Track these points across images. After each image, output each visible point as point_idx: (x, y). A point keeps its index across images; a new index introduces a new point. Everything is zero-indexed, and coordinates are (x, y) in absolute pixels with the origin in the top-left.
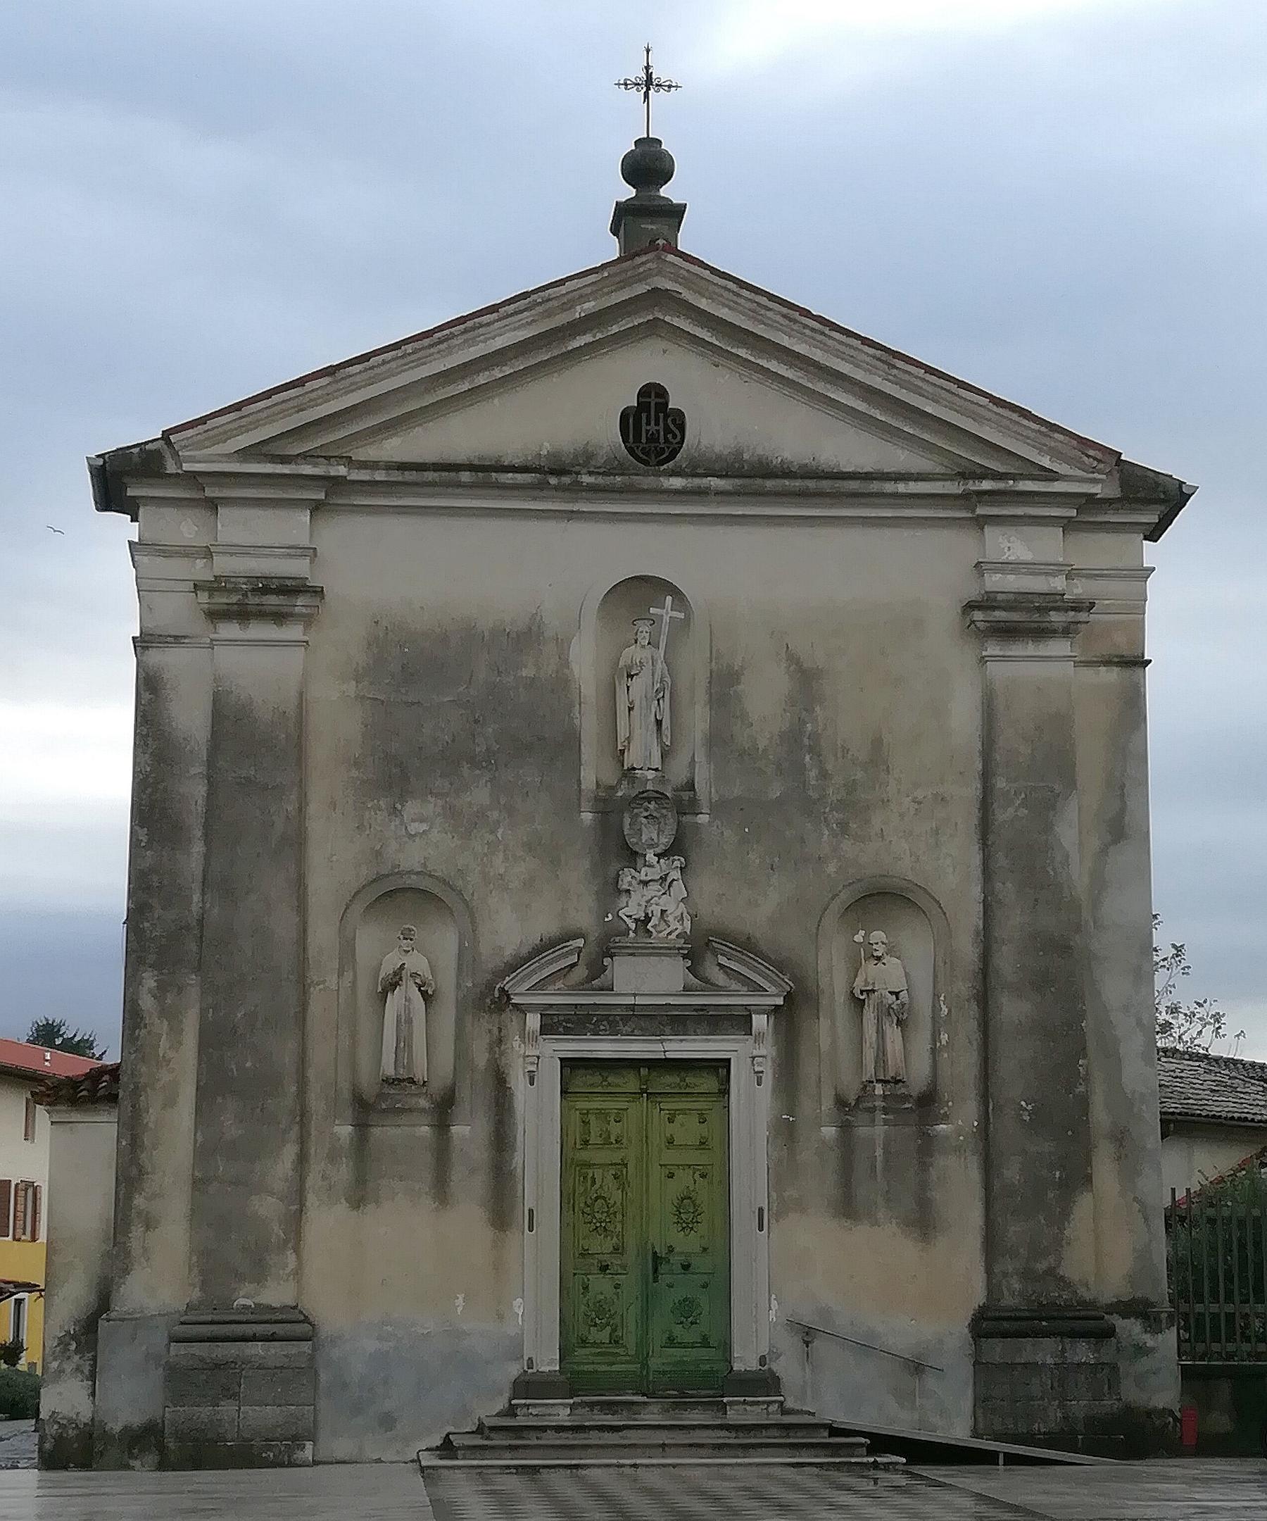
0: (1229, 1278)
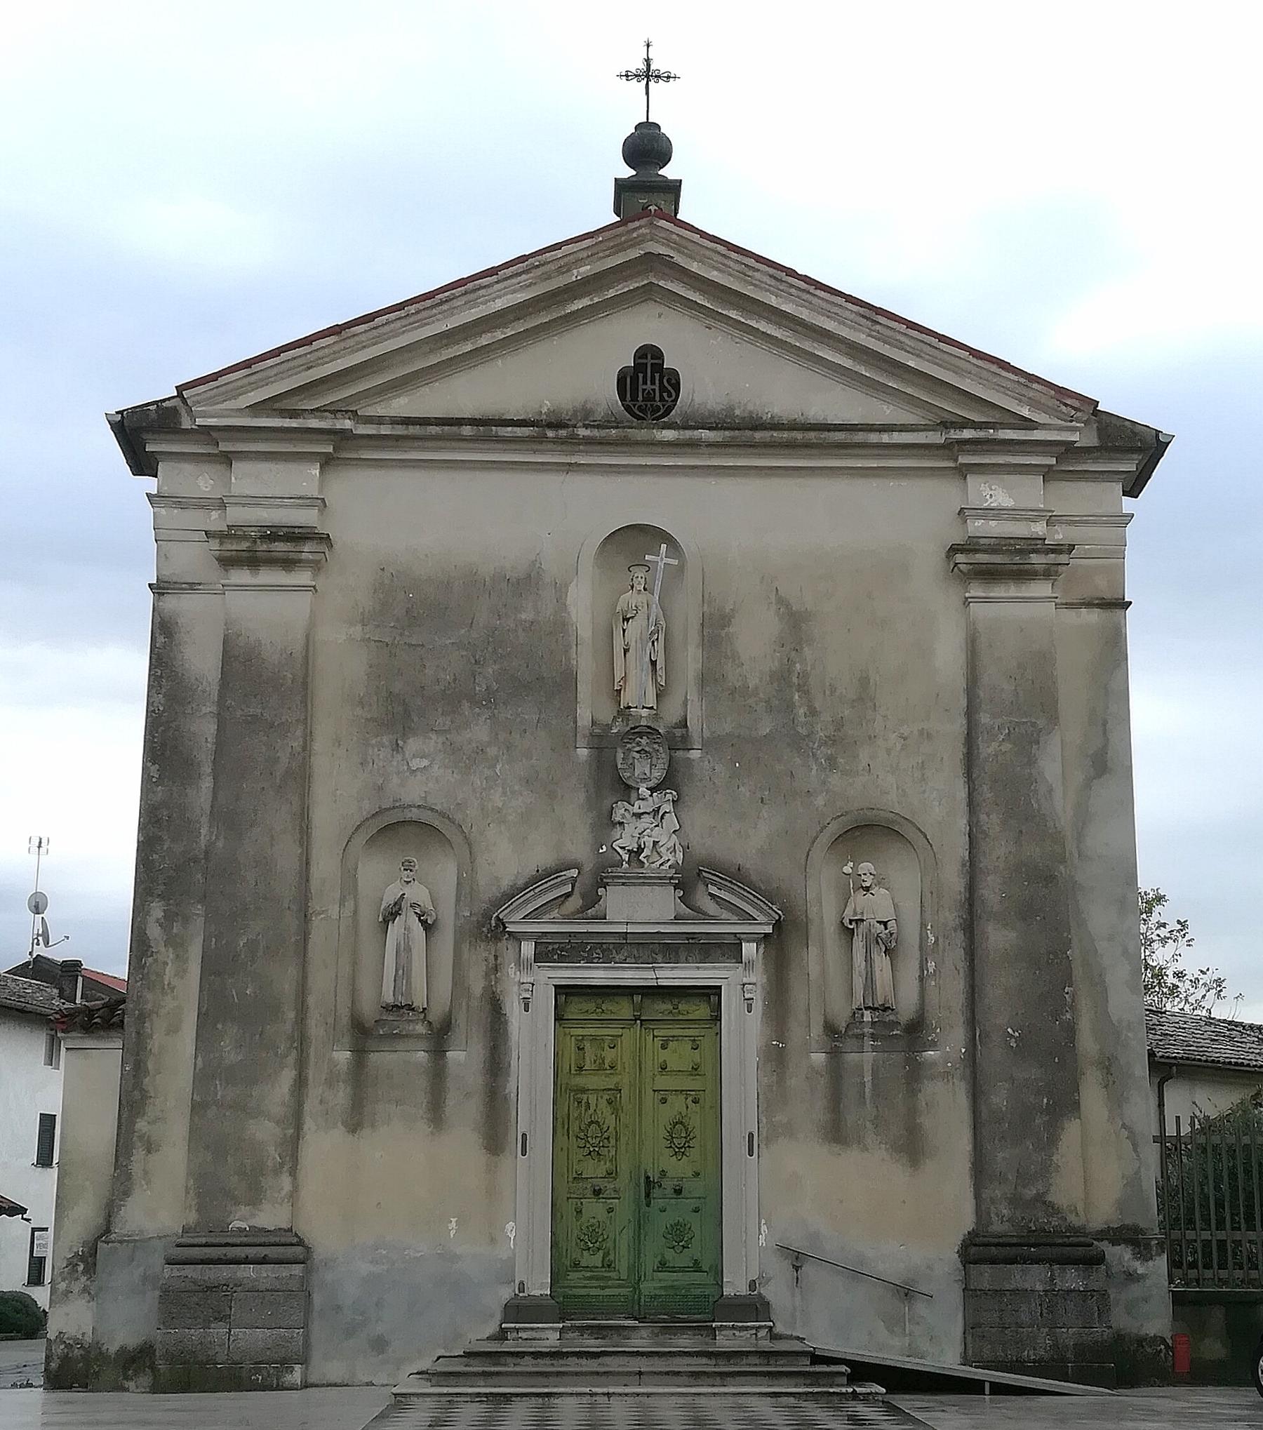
0: (1220, 1205)
